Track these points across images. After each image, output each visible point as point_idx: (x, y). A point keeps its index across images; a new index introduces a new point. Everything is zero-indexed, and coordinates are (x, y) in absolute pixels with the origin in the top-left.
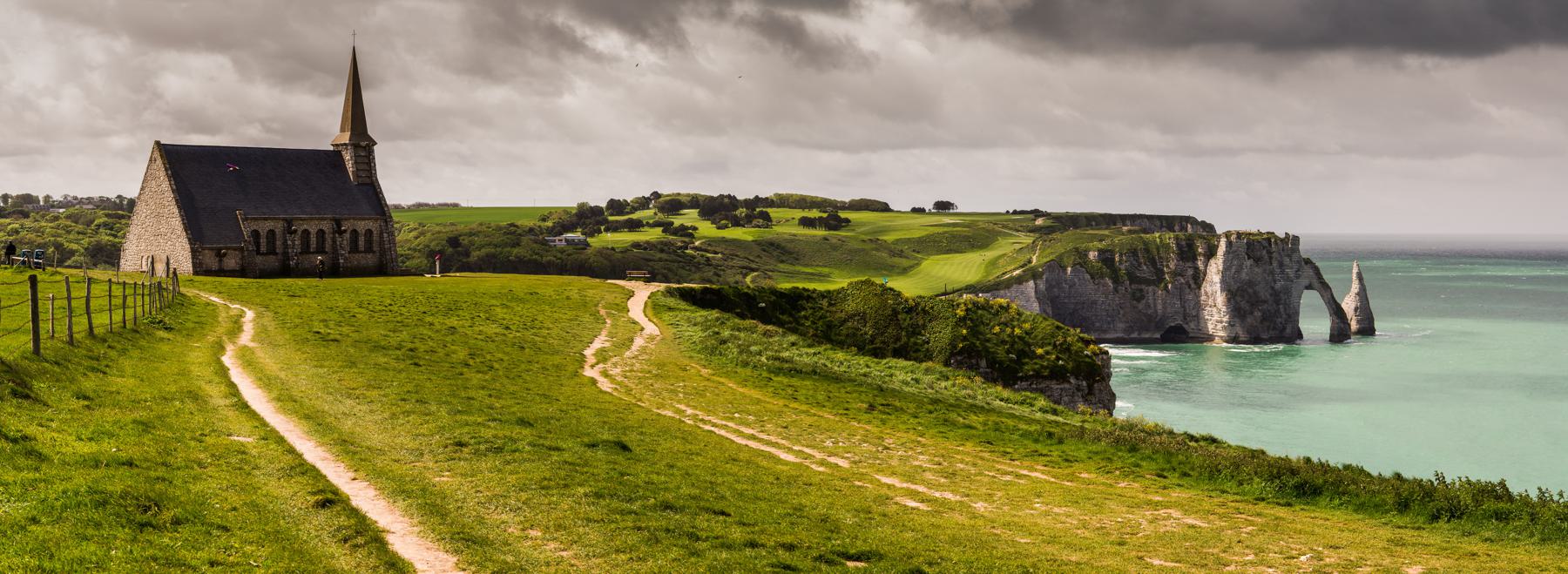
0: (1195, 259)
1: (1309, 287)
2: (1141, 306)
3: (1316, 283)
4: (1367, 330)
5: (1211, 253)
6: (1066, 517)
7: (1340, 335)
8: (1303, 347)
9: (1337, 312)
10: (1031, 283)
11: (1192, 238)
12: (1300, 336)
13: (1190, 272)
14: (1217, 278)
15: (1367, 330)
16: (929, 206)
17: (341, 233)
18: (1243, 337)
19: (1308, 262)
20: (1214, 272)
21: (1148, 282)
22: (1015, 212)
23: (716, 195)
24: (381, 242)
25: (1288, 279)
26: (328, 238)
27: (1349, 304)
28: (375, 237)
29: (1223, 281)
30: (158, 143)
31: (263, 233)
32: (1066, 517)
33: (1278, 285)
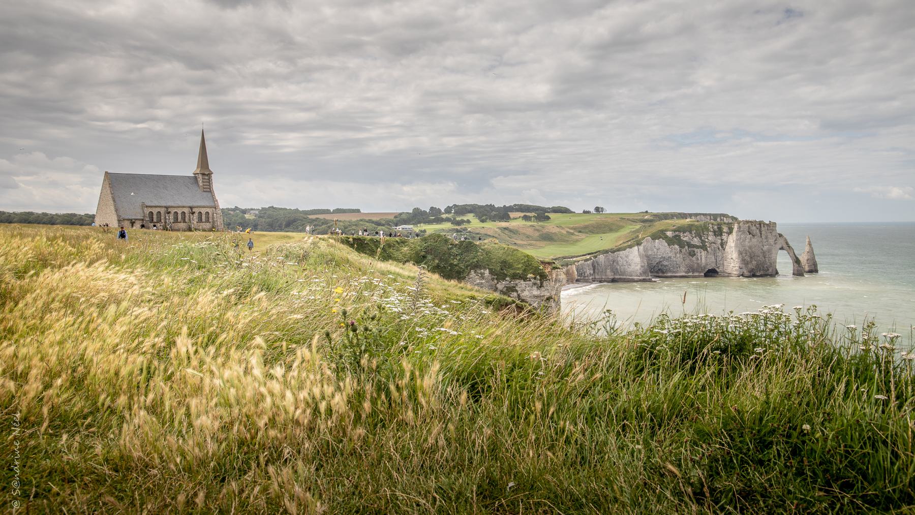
0: (721, 235)
1: (782, 248)
2: (694, 259)
3: (785, 246)
4: (814, 270)
5: (730, 232)
6: (355, 258)
7: (799, 273)
8: (778, 279)
9: (797, 261)
10: (636, 248)
11: (720, 225)
12: (777, 273)
13: (719, 241)
14: (733, 245)
15: (814, 270)
16: (592, 210)
17: (193, 213)
18: (746, 273)
19: (780, 235)
20: (732, 241)
21: (698, 247)
22: (338, 211)
23: (83, 214)
24: (213, 218)
25: (771, 245)
26: (187, 215)
27: (803, 258)
28: (210, 215)
29: (736, 246)
30: (106, 173)
31: (155, 213)
32: (355, 258)
33: (765, 248)
